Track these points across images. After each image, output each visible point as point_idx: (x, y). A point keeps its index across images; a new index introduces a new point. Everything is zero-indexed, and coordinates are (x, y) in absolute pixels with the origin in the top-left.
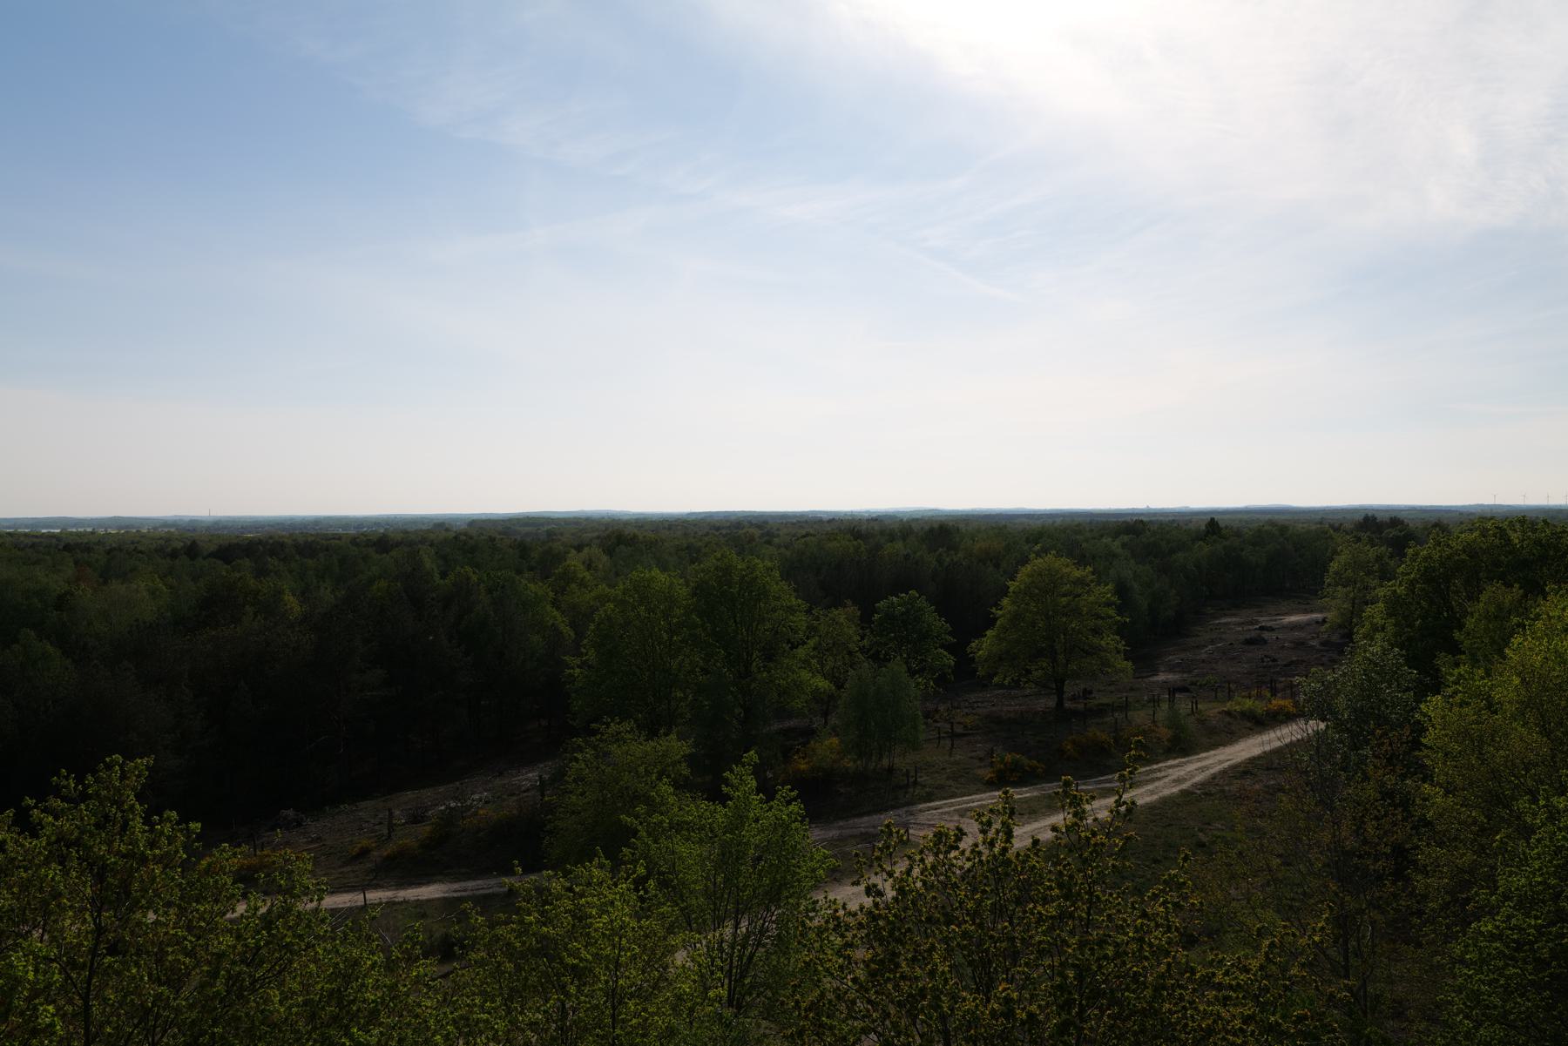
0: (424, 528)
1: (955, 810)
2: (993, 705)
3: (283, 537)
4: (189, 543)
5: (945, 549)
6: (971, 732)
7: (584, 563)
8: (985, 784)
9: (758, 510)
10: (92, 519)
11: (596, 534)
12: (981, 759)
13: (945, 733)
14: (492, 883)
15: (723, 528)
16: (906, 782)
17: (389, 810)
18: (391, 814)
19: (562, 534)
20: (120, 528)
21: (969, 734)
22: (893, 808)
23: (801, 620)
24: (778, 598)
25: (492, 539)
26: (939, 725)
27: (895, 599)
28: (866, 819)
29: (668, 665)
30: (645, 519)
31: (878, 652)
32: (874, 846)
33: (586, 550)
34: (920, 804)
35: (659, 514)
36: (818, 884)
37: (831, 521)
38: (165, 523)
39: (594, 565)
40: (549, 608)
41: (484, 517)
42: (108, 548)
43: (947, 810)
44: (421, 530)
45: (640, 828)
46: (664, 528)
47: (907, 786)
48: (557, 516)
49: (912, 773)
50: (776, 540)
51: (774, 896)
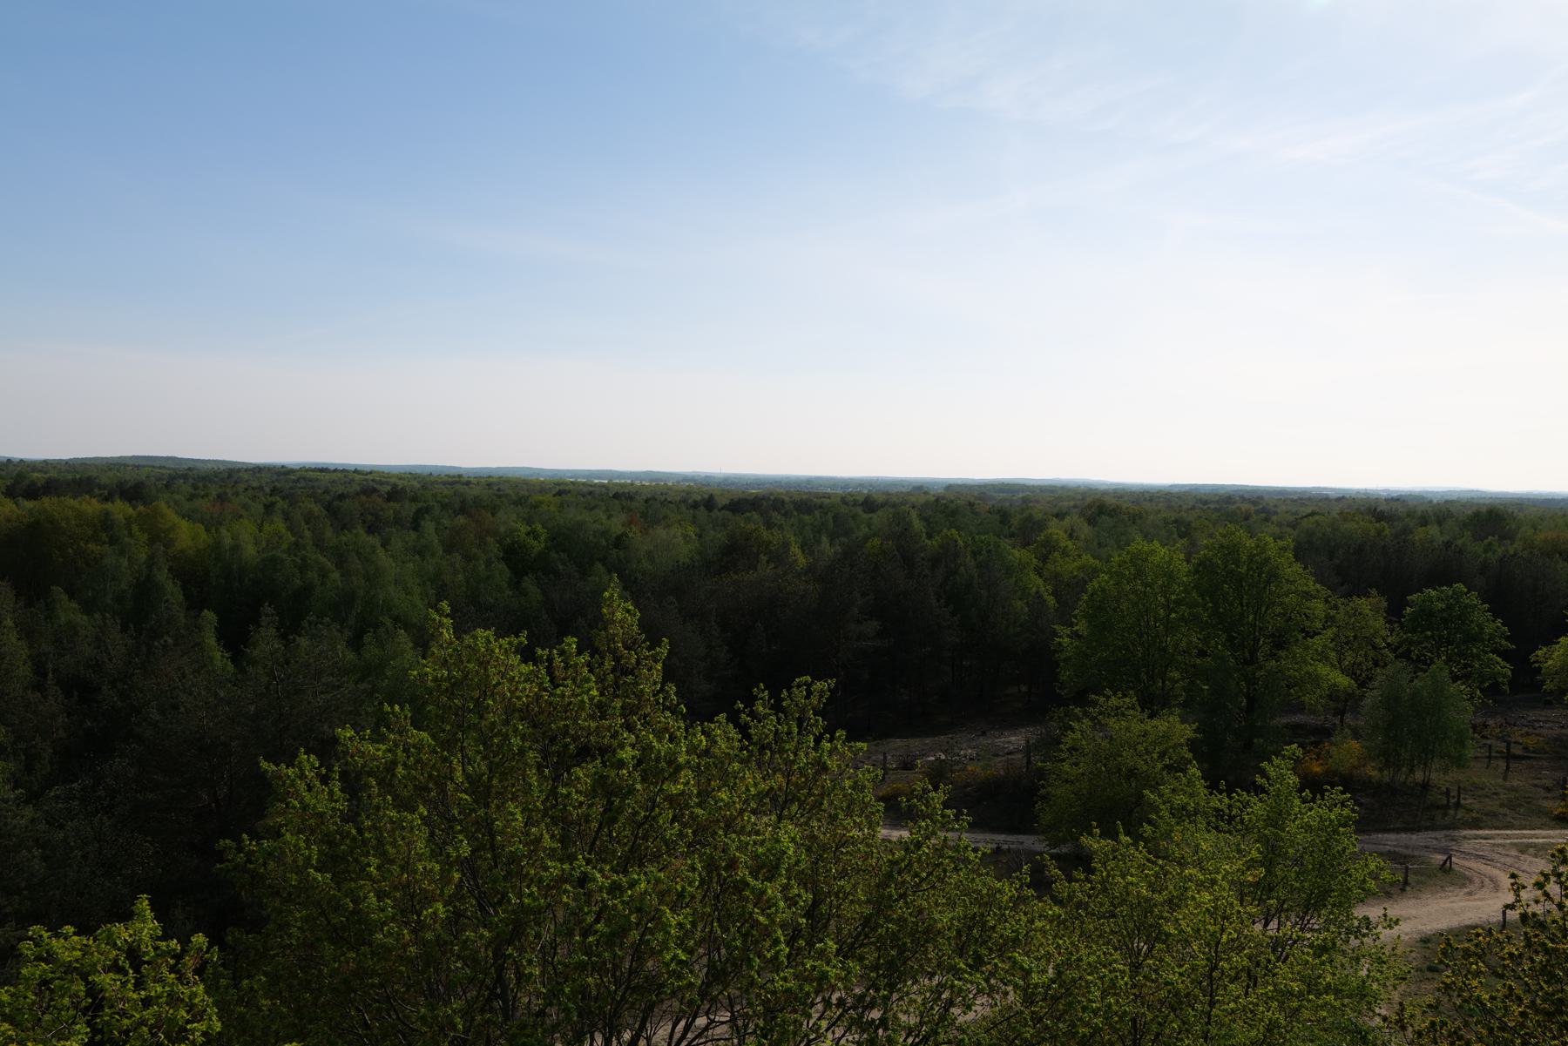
0: (904, 490)
1: (1512, 844)
2: (1562, 727)
3: (782, 493)
4: (706, 497)
5: (1497, 537)
6: (1532, 755)
7: (1066, 532)
8: (1553, 819)
9: (1251, 484)
10: (631, 473)
11: (1072, 503)
12: (1548, 789)
13: (1497, 752)
14: (980, 838)
15: (1212, 502)
16: (1445, 802)
17: (885, 754)
18: (885, 758)
19: (1038, 502)
20: (651, 481)
21: (1532, 758)
22: (1427, 829)
23: (1319, 608)
24: (1292, 582)
25: (971, 504)
26: (1489, 742)
27: (1433, 593)
28: (1392, 836)
29: (1164, 644)
30: (1124, 489)
31: (1409, 651)
32: (1407, 868)
33: (1068, 519)
34: (1465, 830)
35: (1138, 485)
36: (1368, 896)
37: (1341, 499)
38: (686, 478)
39: (1075, 534)
40: (1032, 575)
41: (960, 482)
42: (645, 498)
43: (1501, 841)
44: (902, 492)
45: (1162, 807)
46: (1145, 500)
47: (1447, 806)
48: (1031, 483)
49: (1454, 793)
50: (1274, 518)
51: (1313, 903)
